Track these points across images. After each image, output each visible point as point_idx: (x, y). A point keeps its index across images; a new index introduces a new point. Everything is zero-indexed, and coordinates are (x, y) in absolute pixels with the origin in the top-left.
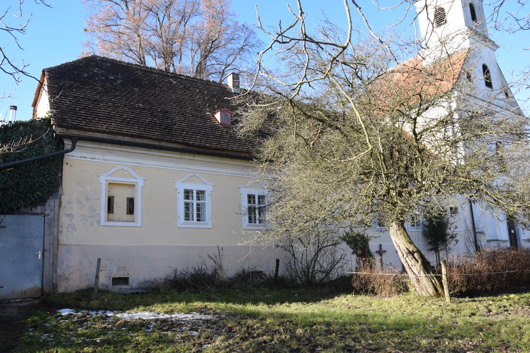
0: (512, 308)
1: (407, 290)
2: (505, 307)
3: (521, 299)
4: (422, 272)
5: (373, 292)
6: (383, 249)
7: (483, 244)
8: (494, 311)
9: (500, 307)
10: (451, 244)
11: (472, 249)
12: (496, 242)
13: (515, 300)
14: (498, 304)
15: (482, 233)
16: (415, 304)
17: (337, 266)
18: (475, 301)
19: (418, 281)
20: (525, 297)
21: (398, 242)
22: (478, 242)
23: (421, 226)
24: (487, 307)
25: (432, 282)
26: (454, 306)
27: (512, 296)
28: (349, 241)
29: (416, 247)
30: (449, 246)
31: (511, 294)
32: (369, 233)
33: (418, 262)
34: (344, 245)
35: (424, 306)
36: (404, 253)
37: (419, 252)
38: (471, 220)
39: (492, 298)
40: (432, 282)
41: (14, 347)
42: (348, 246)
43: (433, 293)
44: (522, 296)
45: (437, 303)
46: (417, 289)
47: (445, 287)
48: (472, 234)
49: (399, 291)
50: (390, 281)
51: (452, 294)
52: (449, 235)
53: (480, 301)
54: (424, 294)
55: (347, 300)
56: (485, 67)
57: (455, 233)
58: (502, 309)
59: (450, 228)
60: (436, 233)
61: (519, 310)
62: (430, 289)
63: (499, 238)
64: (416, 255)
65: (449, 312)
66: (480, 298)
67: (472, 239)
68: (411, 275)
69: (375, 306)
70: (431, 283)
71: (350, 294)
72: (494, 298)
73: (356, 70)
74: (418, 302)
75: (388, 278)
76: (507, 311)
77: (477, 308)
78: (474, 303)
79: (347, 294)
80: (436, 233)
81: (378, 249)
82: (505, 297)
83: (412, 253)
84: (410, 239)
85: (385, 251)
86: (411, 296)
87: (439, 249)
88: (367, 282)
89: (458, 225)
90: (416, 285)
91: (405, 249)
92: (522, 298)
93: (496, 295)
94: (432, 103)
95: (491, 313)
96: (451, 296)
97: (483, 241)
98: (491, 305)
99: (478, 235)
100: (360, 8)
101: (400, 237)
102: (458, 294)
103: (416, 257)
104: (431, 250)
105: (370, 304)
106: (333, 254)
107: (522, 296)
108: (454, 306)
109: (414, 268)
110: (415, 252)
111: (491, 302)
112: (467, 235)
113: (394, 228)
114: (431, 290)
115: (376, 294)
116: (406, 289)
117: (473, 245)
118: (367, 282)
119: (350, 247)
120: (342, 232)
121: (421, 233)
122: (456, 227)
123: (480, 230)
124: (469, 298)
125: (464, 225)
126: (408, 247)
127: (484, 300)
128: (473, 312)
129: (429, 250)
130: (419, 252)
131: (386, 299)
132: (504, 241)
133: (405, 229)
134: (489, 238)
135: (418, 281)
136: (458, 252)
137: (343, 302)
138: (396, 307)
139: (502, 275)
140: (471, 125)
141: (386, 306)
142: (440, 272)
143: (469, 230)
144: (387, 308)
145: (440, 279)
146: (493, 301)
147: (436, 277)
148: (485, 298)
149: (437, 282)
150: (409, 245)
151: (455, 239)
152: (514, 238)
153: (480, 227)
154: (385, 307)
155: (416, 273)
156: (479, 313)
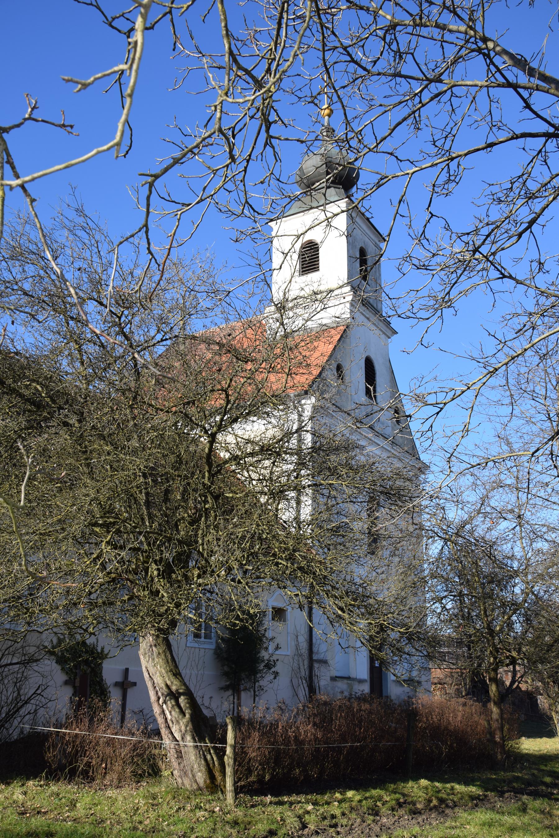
0: (344, 821)
1: (155, 772)
2: (333, 817)
3: (364, 802)
4: (188, 738)
5: (87, 776)
6: (131, 678)
7: (323, 683)
8: (312, 827)
9: (324, 818)
10: (265, 680)
11: (303, 692)
12: (346, 681)
13: (354, 804)
14: (322, 810)
15: (324, 662)
16: (165, 806)
17: (22, 712)
18: (281, 803)
19: (180, 755)
20: (371, 797)
21: (151, 670)
22: (315, 679)
23: (213, 640)
24: (300, 817)
25: (206, 760)
26: (239, 813)
27: (350, 794)
28: (63, 656)
29: (185, 684)
30: (262, 683)
31: (350, 789)
32: (105, 640)
33: (185, 715)
34: (49, 666)
35: (182, 813)
36: (160, 694)
37: (189, 694)
38: (306, 636)
39: (314, 797)
40: (206, 760)
41: (37, 660)
42: (59, 667)
43: (205, 782)
44: (368, 795)
45: (207, 807)
46: (175, 772)
47: (229, 771)
48: (306, 662)
49: (140, 775)
50: (124, 751)
51: (242, 787)
52: (263, 661)
53: (291, 804)
54: (187, 783)
55: (25, 793)
56: (369, 365)
57: (275, 658)
58: (327, 822)
59: (267, 648)
60: (240, 655)
61: (356, 825)
62: (199, 774)
63: (353, 675)
64: (182, 700)
65: (228, 828)
66: (294, 798)
67: (304, 672)
68: (167, 741)
69: (81, 810)
70: (203, 762)
71: (35, 778)
72: (319, 797)
73: (120, 318)
74: (172, 803)
75: (124, 743)
76: (335, 826)
77: (282, 819)
78: (280, 809)
79: (28, 779)
80: (240, 655)
81: (119, 679)
82: (338, 795)
83: (173, 696)
84: (176, 667)
85: (135, 684)
86: (159, 789)
87: (242, 687)
88: (77, 751)
89: (282, 641)
90: (175, 764)
91: (163, 685)
92: (366, 798)
93: (322, 792)
94: (254, 409)
95: (306, 831)
96: (237, 791)
97: (323, 679)
98: (308, 812)
99: (316, 665)
100: (33, 201)
101: (156, 660)
102: (256, 786)
103: (182, 705)
104: (225, 689)
105: (73, 805)
106: (18, 684)
107: (368, 795)
108: (239, 813)
109: (175, 728)
110: (180, 694)
111: (310, 807)
112: (295, 665)
113: (146, 642)
114: (201, 777)
115: (93, 779)
116: (153, 770)
117: (305, 685)
118: (77, 751)
119: (63, 669)
120: (48, 639)
121: (212, 652)
122: (277, 648)
123: (321, 657)
124: (272, 795)
125: (293, 643)
126: (169, 683)
127: (300, 802)
128: (273, 827)
129: (222, 689)
130: (189, 694)
131: (110, 793)
132: (361, 681)
133: (169, 646)
134: (335, 673)
135: (180, 755)
136: (275, 698)
137: (15, 797)
138: (125, 812)
139: (339, 750)
140: (325, 459)
141: (103, 810)
142: (224, 740)
143: (301, 655)
144: (106, 814)
145: (221, 753)
146: (315, 804)
147: (215, 748)
148: (302, 798)
149: (215, 759)
150: (172, 678)
151: (273, 670)
152: (377, 673)
153: (321, 649)
154: (102, 810)
155: (178, 736)
156: (283, 831)
